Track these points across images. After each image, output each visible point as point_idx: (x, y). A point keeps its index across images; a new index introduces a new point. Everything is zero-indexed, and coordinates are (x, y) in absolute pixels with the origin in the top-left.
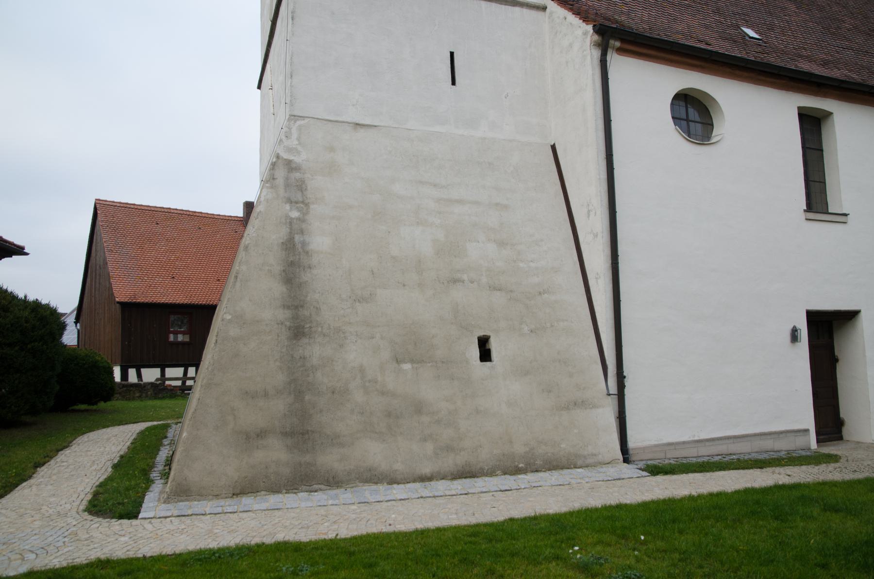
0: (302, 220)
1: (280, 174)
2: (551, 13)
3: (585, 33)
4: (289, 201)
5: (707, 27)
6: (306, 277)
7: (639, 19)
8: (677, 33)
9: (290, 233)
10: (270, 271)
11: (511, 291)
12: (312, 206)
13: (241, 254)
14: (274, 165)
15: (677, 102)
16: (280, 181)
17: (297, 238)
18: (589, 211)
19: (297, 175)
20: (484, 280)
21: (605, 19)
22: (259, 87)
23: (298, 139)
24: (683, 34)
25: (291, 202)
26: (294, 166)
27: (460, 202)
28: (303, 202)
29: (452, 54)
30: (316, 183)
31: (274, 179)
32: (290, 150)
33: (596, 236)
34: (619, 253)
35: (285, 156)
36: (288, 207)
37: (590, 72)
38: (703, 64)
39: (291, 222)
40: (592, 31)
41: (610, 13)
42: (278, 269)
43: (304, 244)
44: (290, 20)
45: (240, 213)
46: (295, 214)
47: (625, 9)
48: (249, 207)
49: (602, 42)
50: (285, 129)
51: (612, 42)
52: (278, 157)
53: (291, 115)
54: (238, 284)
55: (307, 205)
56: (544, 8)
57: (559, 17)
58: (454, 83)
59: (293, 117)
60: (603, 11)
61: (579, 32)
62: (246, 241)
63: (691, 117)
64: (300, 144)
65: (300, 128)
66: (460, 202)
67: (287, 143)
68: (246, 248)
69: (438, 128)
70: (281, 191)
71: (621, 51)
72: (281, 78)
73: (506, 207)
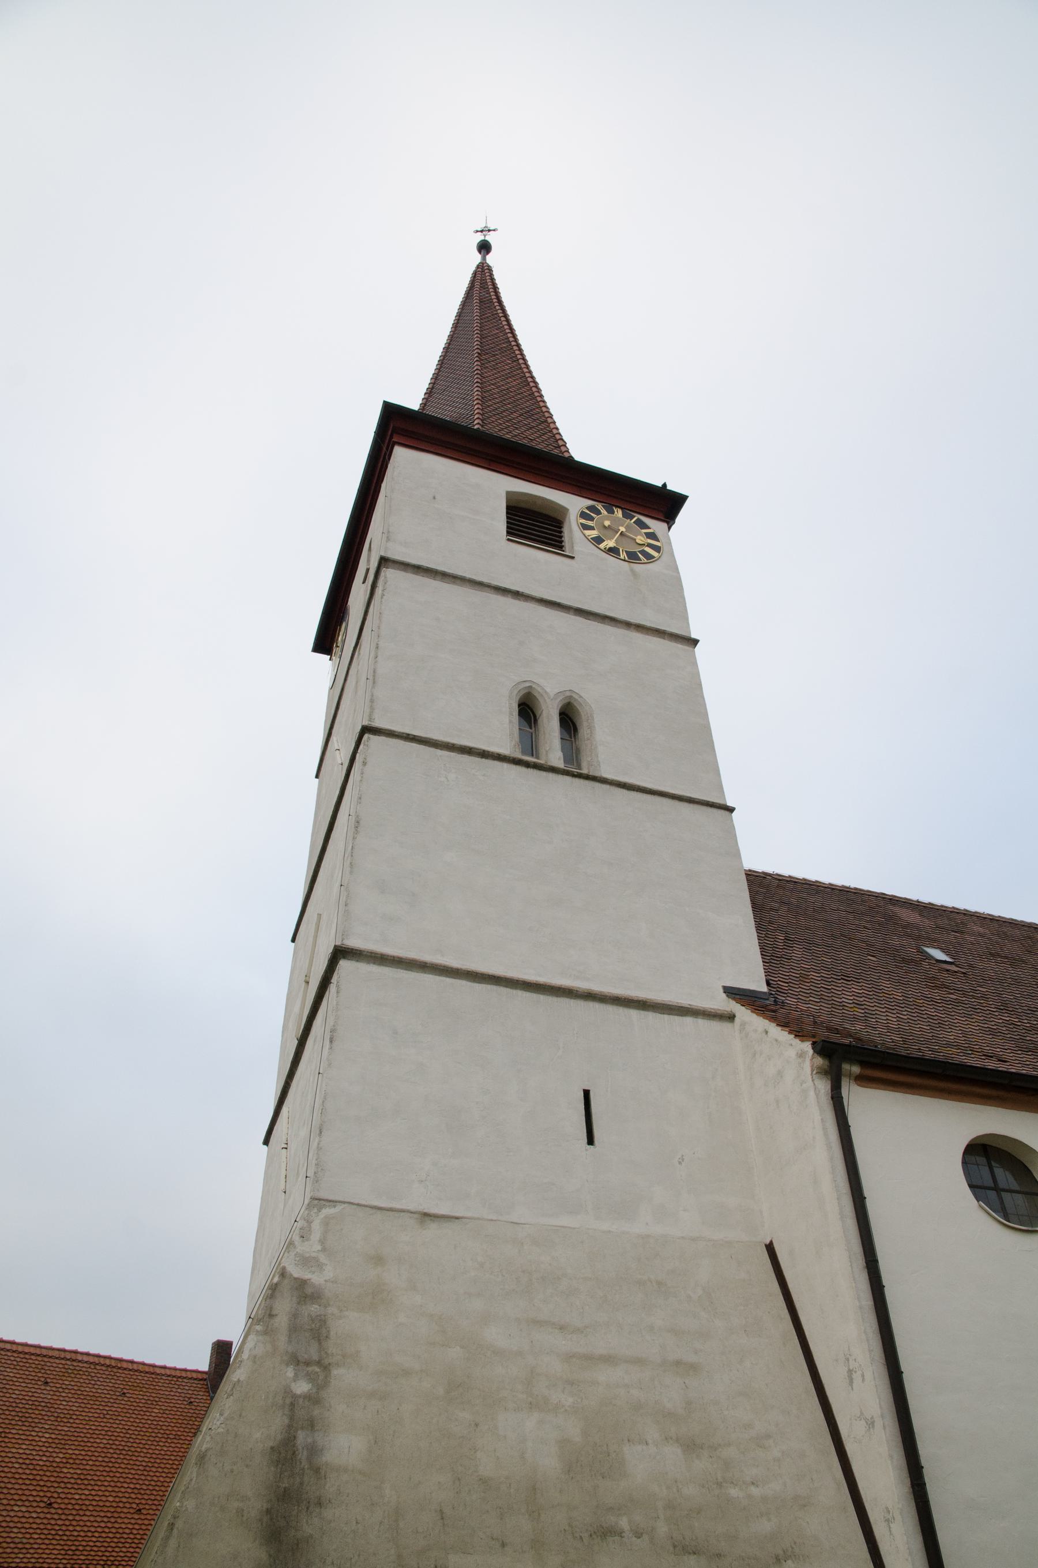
0: (314, 1399)
1: (284, 1306)
2: (743, 1024)
3: (801, 1055)
4: (295, 1360)
5: (993, 1033)
6: (309, 1526)
7: (885, 1027)
8: (949, 1045)
9: (290, 1426)
10: (240, 1512)
11: (719, 1555)
12: (335, 1372)
13: (190, 1473)
14: (273, 1290)
15: (972, 1159)
16: (282, 1321)
17: (302, 1438)
18: (850, 1372)
19: (314, 1309)
20: (662, 1529)
21: (830, 1029)
22: (266, 1142)
23: (322, 1242)
24: (958, 1047)
25: (298, 1363)
26: (309, 1290)
27: (609, 1360)
28: (319, 1363)
29: (587, 1094)
30: (348, 1324)
31: (271, 1316)
32: (305, 1261)
33: (871, 1424)
34: (866, 1193)
35: (296, 1272)
36: (290, 1372)
37: (817, 1117)
38: (1001, 1093)
39: (292, 1404)
40: (811, 1052)
41: (836, 1020)
42: (255, 1507)
43: (314, 1450)
44: (347, 869)
45: (201, 1362)
46: (302, 1387)
47: (859, 1012)
48: (222, 1351)
49: (830, 1067)
50: (301, 1223)
51: (846, 1067)
52: (283, 1274)
53: (313, 1199)
54: (173, 1543)
55: (326, 1368)
56: (731, 1017)
57: (756, 1031)
58: (591, 1141)
59: (317, 1202)
60: (824, 1018)
61: (791, 1053)
62: (202, 1442)
63: (1002, 1184)
64: (324, 1250)
65: (326, 1222)
66: (609, 1360)
67: (301, 1247)
68: (202, 1457)
69: (565, 1221)
70: (282, 1339)
71: (862, 1080)
72: (304, 1132)
73: (693, 1368)
